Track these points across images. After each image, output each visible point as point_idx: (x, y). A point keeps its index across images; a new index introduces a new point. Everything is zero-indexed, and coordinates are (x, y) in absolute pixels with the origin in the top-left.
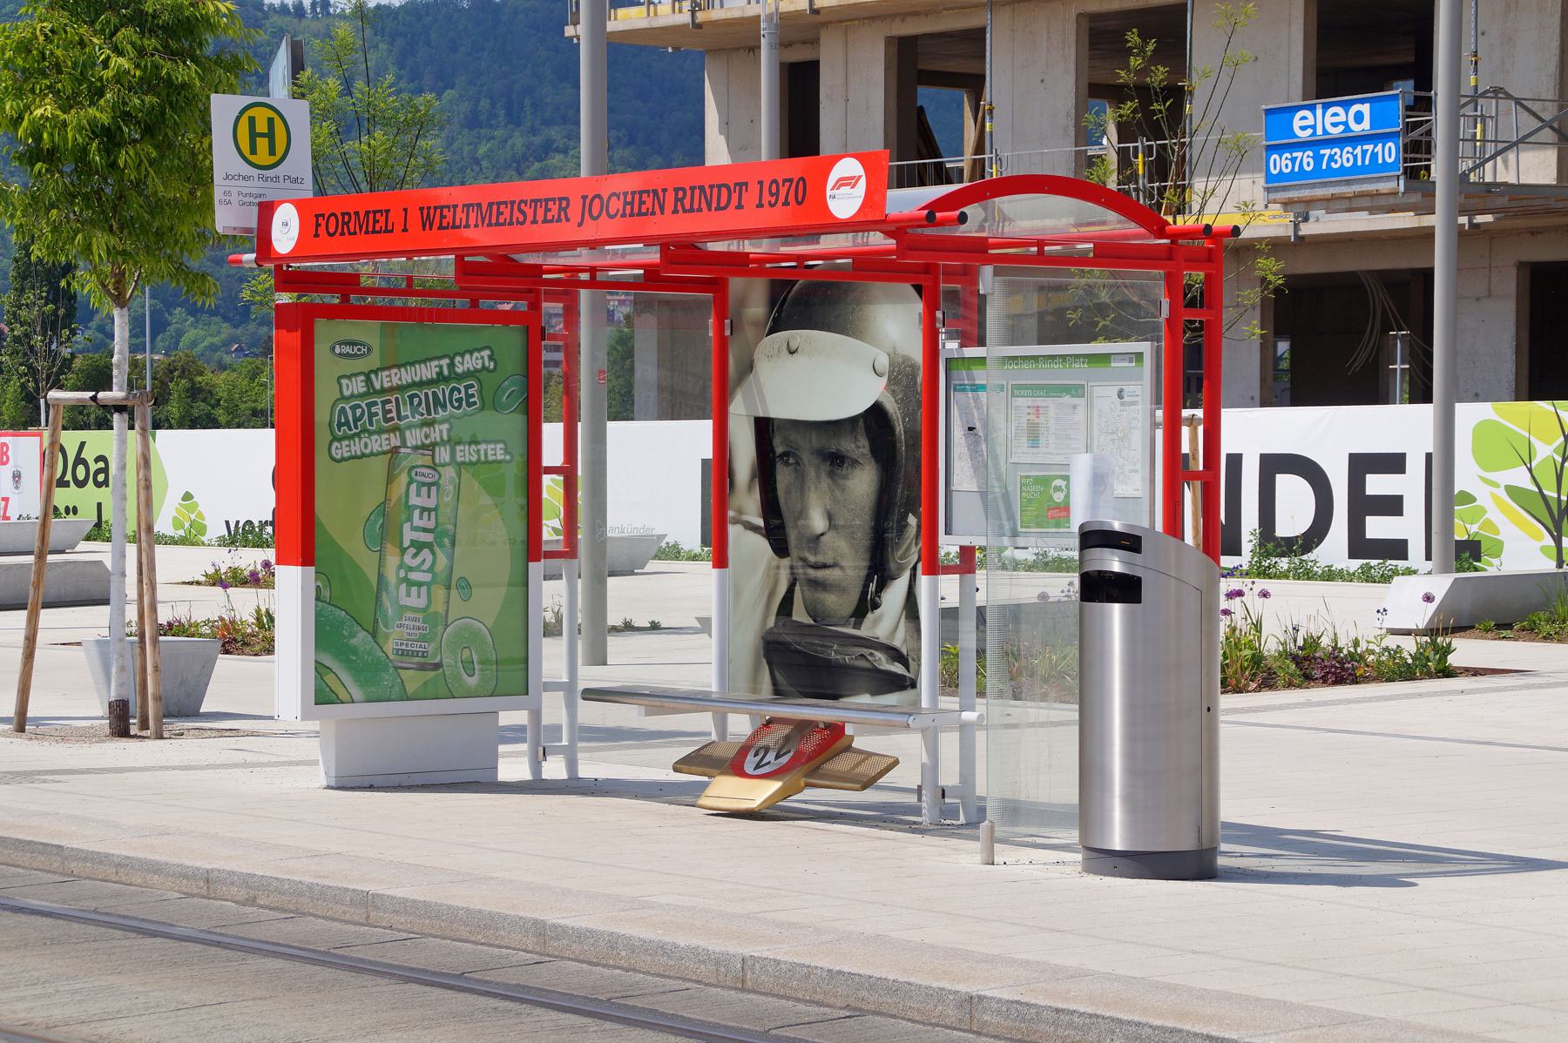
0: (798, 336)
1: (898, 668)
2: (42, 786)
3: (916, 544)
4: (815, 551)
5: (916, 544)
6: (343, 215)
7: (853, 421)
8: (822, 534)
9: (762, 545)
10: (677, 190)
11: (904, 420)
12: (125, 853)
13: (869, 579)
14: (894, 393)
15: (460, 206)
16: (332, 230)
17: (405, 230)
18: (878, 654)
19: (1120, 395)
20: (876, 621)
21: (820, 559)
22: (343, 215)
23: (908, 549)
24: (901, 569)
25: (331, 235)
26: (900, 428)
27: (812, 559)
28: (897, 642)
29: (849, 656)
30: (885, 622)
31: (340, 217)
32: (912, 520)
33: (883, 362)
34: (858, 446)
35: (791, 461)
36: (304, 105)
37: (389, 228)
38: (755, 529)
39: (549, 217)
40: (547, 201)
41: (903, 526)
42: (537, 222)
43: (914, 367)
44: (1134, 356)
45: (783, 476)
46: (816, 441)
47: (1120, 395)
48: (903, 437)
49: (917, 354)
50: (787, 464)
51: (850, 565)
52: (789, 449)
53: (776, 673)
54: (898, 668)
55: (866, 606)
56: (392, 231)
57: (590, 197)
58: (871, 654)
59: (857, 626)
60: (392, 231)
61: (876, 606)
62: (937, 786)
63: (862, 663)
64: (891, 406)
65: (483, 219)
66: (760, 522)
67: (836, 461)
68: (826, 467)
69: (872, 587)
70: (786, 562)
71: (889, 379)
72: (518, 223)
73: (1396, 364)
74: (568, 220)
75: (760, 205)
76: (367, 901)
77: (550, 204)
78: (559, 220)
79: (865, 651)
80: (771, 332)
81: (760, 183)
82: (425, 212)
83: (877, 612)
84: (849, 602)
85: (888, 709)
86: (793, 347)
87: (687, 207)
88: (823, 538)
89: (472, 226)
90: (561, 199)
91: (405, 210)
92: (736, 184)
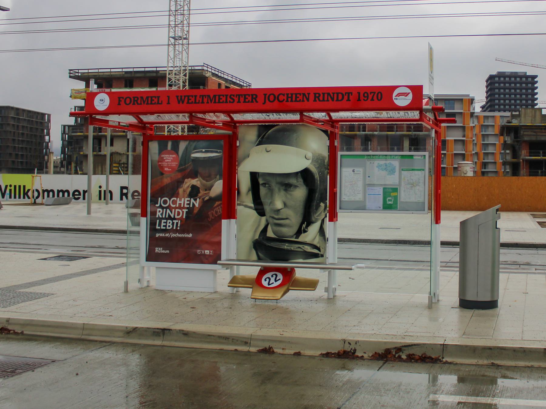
1: (316, 251)
2: (203, 290)
3: (324, 212)
4: (278, 214)
5: (324, 212)
6: (134, 98)
7: (296, 174)
8: (281, 209)
9: (254, 213)
11: (319, 174)
13: (302, 223)
14: (314, 165)
15: (198, 96)
17: (169, 103)
21: (280, 217)
22: (134, 98)
23: (321, 213)
25: (127, 104)
26: (317, 176)
27: (276, 217)
28: (316, 242)
29: (294, 247)
31: (132, 99)
32: (322, 205)
33: (310, 155)
35: (267, 186)
37: (160, 102)
38: (250, 207)
39: (190, 101)
40: (245, 95)
41: (318, 206)
42: (204, 103)
44: (423, 156)
45: (263, 191)
46: (279, 179)
47: (353, 171)
48: (318, 179)
49: (325, 153)
50: (265, 187)
52: (266, 182)
54: (316, 251)
56: (161, 103)
57: (268, 95)
58: (303, 247)
59: (297, 237)
60: (161, 103)
62: (141, 283)
63: (299, 250)
64: (313, 169)
65: (211, 101)
66: (252, 205)
67: (287, 187)
68: (283, 188)
71: (312, 160)
72: (230, 102)
74: (257, 102)
78: (252, 102)
79: (301, 246)
80: (258, 145)
83: (306, 234)
84: (295, 229)
85: (449, 264)
86: (268, 150)
88: (281, 210)
89: (205, 103)
90: (252, 95)
92: (346, 93)
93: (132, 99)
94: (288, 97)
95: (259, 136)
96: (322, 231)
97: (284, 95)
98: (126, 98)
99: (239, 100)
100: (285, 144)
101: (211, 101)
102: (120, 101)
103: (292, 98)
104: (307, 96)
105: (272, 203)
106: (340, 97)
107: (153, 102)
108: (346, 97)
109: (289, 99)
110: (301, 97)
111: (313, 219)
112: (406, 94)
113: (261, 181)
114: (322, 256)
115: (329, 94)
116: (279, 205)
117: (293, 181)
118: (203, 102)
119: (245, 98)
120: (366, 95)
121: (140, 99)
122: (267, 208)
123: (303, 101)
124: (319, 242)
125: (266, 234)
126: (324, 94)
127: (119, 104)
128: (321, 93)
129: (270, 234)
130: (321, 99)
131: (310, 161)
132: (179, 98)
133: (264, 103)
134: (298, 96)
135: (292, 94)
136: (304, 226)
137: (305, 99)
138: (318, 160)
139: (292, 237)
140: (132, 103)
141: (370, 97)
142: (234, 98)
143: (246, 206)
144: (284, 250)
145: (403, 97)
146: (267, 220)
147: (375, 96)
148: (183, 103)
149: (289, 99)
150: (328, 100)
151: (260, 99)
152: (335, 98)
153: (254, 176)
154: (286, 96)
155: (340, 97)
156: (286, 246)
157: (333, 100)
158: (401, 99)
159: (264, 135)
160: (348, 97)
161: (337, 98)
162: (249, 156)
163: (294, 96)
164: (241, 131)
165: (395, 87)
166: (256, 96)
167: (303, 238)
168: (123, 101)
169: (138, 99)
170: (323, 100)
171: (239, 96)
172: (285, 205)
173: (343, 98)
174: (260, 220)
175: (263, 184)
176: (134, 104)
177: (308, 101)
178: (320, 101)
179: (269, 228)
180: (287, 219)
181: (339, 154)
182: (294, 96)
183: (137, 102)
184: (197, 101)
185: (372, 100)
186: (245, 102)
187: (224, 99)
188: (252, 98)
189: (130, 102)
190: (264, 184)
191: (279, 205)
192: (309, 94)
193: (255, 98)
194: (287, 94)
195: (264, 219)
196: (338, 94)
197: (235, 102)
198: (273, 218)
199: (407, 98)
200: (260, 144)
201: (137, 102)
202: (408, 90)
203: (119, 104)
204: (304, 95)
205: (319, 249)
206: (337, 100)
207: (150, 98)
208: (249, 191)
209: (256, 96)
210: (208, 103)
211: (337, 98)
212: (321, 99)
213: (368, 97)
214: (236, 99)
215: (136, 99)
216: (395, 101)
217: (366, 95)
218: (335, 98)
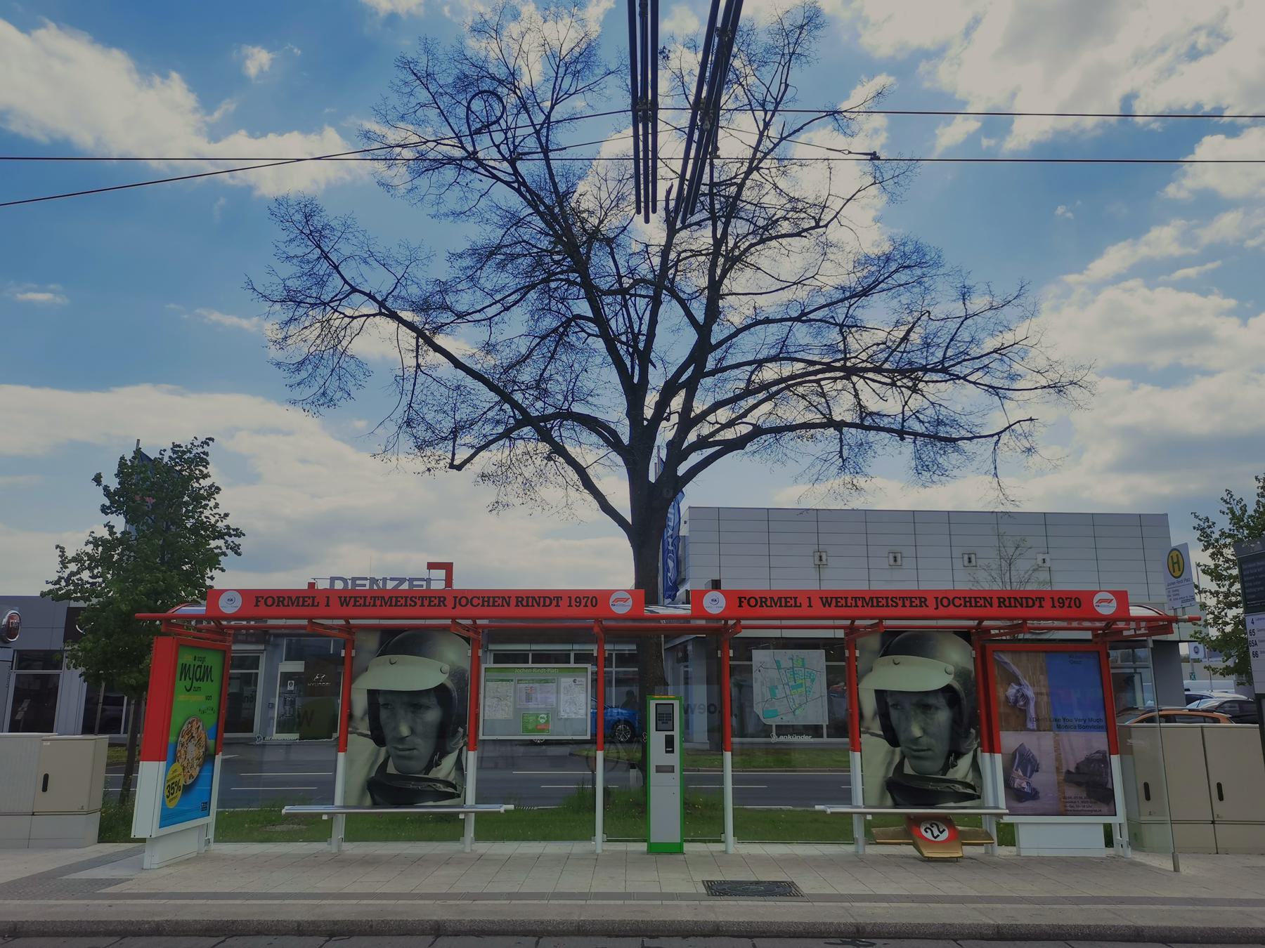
0: (395, 658)
6: (279, 598)
7: (428, 692)
9: (884, 745)
10: (999, 598)
12: (746, 920)
14: (452, 680)
16: (1077, 601)
17: (328, 605)
18: (439, 785)
19: (574, 681)
20: (439, 771)
24: (455, 749)
25: (750, 605)
26: (455, 694)
27: (400, 747)
28: (969, 780)
29: (941, 787)
30: (446, 768)
34: (941, 701)
36: (1175, 541)
38: (366, 736)
40: (430, 597)
43: (971, 672)
45: (384, 714)
51: (424, 747)
53: (376, 797)
55: (433, 763)
59: (944, 774)
60: (800, 606)
61: (438, 765)
66: (882, 733)
69: (436, 757)
70: (898, 750)
73: (611, 672)
75: (570, 606)
76: (1060, 927)
77: (839, 600)
78: (439, 605)
79: (430, 784)
80: (882, 656)
81: (1053, 598)
82: (824, 600)
83: (438, 767)
84: (422, 764)
87: (525, 604)
90: (440, 597)
91: (810, 598)
93: (759, 600)
94: (483, 601)
95: (381, 643)
96: (975, 766)
97: (960, 598)
98: (267, 598)
99: (904, 603)
100: (933, 658)
101: (386, 604)
102: (741, 602)
103: (970, 602)
104: (508, 599)
105: (396, 728)
106: (548, 602)
107: (496, 604)
108: (554, 603)
109: (486, 604)
110: (500, 602)
111: (449, 749)
112: (625, 600)
113: (890, 701)
114: (979, 797)
115: (534, 598)
116: (917, 732)
117: (932, 701)
118: (374, 605)
119: (430, 602)
120: (578, 600)
121: (769, 600)
122: (902, 738)
123: (503, 606)
124: (455, 779)
125: (903, 770)
126: (527, 598)
127: (740, 606)
128: (757, 597)
129: (391, 769)
130: (524, 603)
131: (952, 676)
132: (824, 600)
133: (937, 608)
134: (358, 599)
135: (489, 598)
136: (436, 757)
137: (987, 604)
138: (961, 675)
139: (937, 773)
140: (759, 604)
141: (583, 602)
142: (897, 601)
143: (873, 734)
144: (928, 790)
145: (1106, 604)
146: (387, 752)
147: (589, 602)
148: (830, 606)
149: (486, 604)
150: (533, 606)
151: (931, 602)
152: (542, 604)
153: (880, 694)
154: (481, 599)
155: (548, 602)
156: (930, 786)
157: (539, 605)
158: (1105, 606)
159: (890, 643)
160: (1040, 602)
161: (544, 603)
162: (871, 670)
163: (491, 599)
164: (360, 637)
165: (612, 592)
166: (445, 598)
167: (433, 774)
168: (746, 602)
169: (1005, 600)
170: (527, 605)
171: (903, 598)
172: (413, 731)
173: (551, 603)
174: (379, 750)
175: (893, 705)
176: (278, 605)
177: (991, 606)
178: (284, 605)
179: (391, 764)
180: (929, 750)
181: (483, 666)
182: (491, 599)
183: (766, 605)
184: (367, 604)
185: (586, 606)
186: (429, 605)
187: (403, 602)
188: (440, 601)
189: (941, 601)
190: (895, 706)
191: (404, 731)
192: (991, 598)
193: (443, 602)
194: (483, 598)
195: (383, 750)
196: (544, 598)
197: (899, 607)
198: (396, 748)
199: (1110, 604)
200: (382, 653)
201: (766, 605)
202: (1111, 597)
203: (740, 606)
204: (504, 598)
205: (454, 787)
206: (544, 605)
207: (783, 599)
208: (365, 715)
209: (445, 598)
210: (381, 606)
211: (544, 603)
212: (524, 603)
213: (580, 602)
214: (900, 603)
215: (281, 599)
216: (613, 608)
217: (578, 600)
218: (542, 604)
